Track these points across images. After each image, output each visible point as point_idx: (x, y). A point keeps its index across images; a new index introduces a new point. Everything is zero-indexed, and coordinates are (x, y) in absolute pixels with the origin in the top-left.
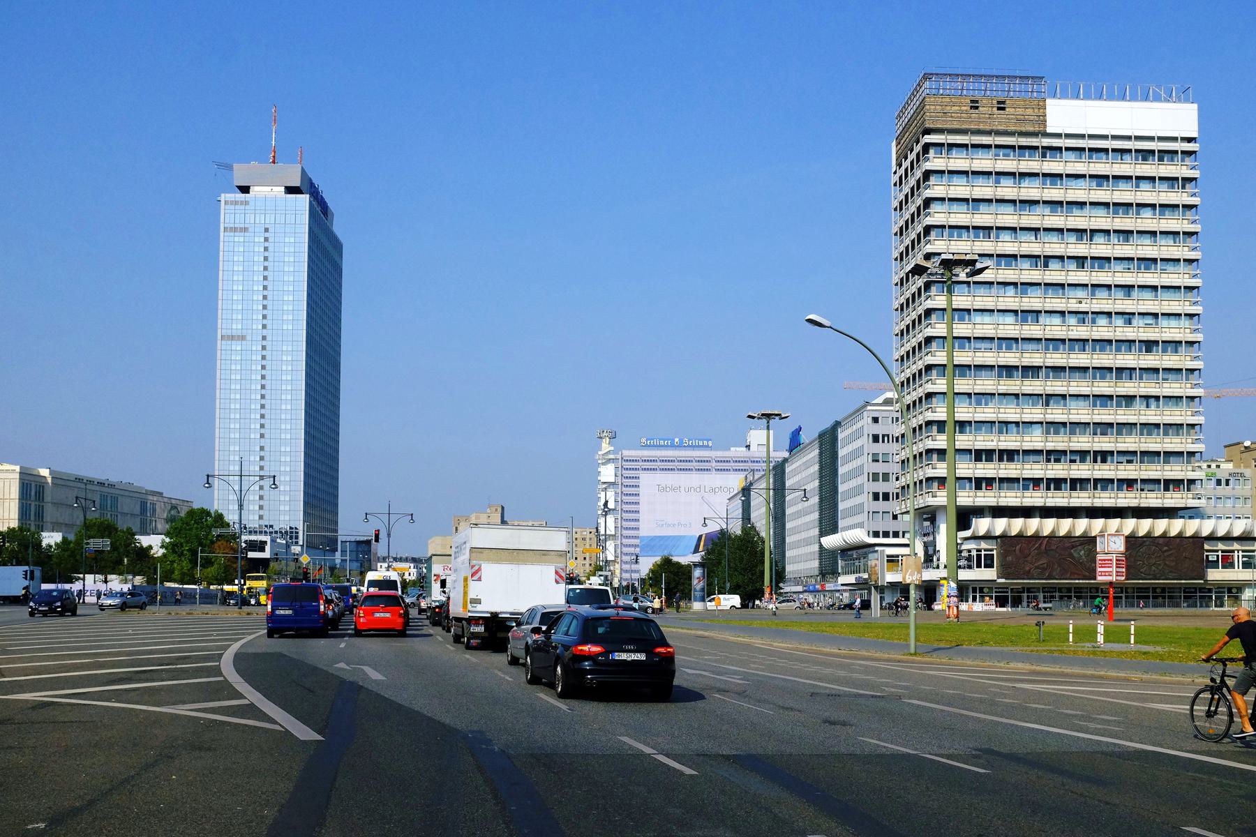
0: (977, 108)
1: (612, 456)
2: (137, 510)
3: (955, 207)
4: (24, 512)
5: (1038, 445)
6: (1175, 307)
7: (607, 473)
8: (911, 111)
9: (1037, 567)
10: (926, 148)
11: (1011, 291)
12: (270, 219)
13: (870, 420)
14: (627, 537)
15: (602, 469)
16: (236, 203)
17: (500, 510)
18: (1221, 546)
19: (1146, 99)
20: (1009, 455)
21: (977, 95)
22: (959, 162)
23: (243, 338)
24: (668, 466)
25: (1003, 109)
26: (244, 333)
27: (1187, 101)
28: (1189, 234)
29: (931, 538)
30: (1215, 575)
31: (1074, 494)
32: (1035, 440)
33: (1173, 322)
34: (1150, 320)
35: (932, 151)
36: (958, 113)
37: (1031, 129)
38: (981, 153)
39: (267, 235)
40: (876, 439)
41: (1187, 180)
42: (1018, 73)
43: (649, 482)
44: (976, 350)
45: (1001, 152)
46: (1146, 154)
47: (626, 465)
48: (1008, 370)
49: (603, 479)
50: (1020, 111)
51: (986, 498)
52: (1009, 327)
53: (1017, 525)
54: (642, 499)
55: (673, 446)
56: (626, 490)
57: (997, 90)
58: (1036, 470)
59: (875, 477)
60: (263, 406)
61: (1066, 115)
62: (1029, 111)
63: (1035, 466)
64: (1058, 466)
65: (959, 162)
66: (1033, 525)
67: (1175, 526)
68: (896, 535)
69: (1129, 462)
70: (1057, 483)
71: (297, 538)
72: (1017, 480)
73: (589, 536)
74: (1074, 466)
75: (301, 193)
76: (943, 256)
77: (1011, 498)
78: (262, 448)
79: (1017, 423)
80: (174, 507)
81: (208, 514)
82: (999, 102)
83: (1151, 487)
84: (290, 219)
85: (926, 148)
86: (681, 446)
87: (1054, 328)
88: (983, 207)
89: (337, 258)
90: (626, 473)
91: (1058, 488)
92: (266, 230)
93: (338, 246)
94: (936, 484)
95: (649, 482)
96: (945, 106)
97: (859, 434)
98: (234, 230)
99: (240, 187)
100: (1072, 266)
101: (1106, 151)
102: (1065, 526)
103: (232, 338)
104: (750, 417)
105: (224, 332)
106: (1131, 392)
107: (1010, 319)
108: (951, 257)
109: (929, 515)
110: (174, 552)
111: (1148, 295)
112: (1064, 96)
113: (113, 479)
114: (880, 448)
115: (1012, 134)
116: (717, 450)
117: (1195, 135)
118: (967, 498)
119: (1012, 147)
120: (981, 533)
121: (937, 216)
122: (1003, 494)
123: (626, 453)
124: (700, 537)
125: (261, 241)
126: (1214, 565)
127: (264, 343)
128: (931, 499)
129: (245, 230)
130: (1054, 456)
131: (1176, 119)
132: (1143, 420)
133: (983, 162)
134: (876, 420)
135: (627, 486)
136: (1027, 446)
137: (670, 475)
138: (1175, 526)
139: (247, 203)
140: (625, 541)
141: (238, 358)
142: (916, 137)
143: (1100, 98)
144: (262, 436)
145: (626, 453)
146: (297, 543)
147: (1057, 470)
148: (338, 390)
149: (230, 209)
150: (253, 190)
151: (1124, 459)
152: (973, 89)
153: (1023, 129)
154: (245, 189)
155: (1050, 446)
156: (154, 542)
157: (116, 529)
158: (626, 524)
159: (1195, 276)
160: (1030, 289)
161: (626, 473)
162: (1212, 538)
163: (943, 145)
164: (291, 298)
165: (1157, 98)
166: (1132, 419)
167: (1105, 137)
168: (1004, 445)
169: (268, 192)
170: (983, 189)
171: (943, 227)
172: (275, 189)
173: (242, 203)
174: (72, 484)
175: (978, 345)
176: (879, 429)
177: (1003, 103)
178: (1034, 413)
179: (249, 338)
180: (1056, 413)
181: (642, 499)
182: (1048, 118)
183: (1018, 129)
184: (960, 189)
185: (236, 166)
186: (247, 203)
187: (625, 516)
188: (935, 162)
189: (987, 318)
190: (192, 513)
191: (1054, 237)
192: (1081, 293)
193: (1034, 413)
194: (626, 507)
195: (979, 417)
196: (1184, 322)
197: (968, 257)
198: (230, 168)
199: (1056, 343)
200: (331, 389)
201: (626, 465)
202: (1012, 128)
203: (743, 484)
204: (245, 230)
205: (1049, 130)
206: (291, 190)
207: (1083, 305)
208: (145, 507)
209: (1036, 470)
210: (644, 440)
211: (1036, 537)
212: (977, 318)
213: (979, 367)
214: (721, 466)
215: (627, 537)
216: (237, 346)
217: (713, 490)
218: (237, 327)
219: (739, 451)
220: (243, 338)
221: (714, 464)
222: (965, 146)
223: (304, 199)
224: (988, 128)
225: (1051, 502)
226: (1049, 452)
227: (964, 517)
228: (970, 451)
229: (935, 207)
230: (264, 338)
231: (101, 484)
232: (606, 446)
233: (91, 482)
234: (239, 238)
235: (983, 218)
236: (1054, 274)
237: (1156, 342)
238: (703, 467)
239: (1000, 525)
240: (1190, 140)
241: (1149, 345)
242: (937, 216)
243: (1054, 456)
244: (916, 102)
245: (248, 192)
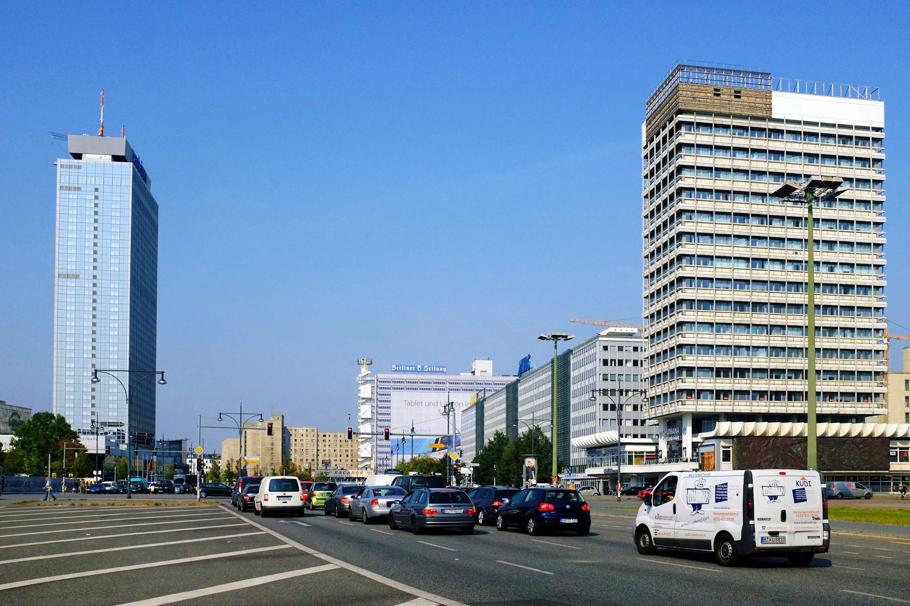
0: (719, 95)
1: (369, 378)
3: (702, 174)
5: (764, 365)
6: (866, 260)
7: (366, 391)
8: (662, 97)
9: (765, 461)
10: (679, 125)
11: (743, 242)
12: (99, 181)
13: (601, 348)
14: (381, 446)
15: (361, 388)
16: (70, 167)
17: (281, 418)
18: (899, 445)
19: (845, 95)
20: (741, 372)
21: (719, 85)
22: (704, 138)
23: (77, 277)
24: (412, 386)
25: (739, 97)
26: (78, 272)
27: (875, 98)
28: (876, 203)
29: (677, 438)
30: (896, 466)
31: (791, 403)
32: (761, 361)
33: (865, 271)
34: (847, 269)
35: (683, 128)
36: (705, 99)
37: (760, 114)
38: (721, 132)
40: (605, 363)
41: (876, 161)
42: (750, 69)
43: (397, 398)
44: (718, 288)
45: (737, 132)
46: (846, 139)
48: (741, 305)
50: (752, 100)
51: (724, 406)
52: (742, 271)
53: (749, 428)
54: (392, 411)
55: (416, 371)
56: (380, 404)
57: (728, 84)
58: (762, 384)
59: (605, 392)
60: (94, 332)
61: (787, 105)
62: (759, 100)
63: (760, 382)
64: (778, 382)
65: (704, 138)
66: (762, 428)
67: (855, 429)
68: (643, 436)
69: (831, 379)
70: (777, 395)
71: (123, 438)
72: (748, 392)
74: (790, 382)
75: (126, 161)
76: (814, 178)
77: (743, 406)
79: (748, 348)
80: (15, 413)
81: (52, 417)
82: (736, 92)
83: (847, 398)
84: (117, 182)
85: (679, 125)
86: (422, 371)
87: (774, 273)
88: (723, 175)
89: (153, 216)
91: (778, 399)
92: (96, 190)
93: (155, 207)
94: (685, 395)
95: (397, 398)
96: (694, 92)
97: (592, 358)
98: (69, 188)
100: (790, 224)
101: (816, 135)
102: (785, 428)
104: (542, 338)
105: (61, 272)
106: (834, 325)
107: (742, 264)
108: (819, 178)
109: (673, 422)
110: (23, 448)
111: (846, 249)
112: (785, 90)
114: (609, 370)
115: (745, 117)
116: (450, 374)
117: (882, 125)
118: (706, 406)
119: (745, 128)
120: (722, 434)
121: (688, 180)
122: (736, 403)
123: (380, 376)
125: (91, 200)
126: (894, 459)
127: (95, 281)
128: (680, 406)
129: (79, 189)
130: (777, 373)
131: (868, 113)
132: (843, 346)
133: (723, 139)
134: (605, 348)
135: (381, 402)
136: (756, 366)
137: (414, 393)
138: (855, 429)
139: (79, 167)
142: (668, 119)
143: (811, 92)
144: (94, 356)
145: (380, 376)
146: (123, 442)
147: (777, 385)
149: (65, 172)
151: (828, 376)
152: (716, 80)
153: (754, 114)
154: (78, 156)
155: (773, 366)
159: (880, 235)
160: (758, 242)
162: (894, 438)
163: (692, 123)
165: (854, 96)
166: (834, 346)
167: (816, 124)
168: (738, 365)
169: (97, 159)
170: (723, 161)
171: (693, 189)
172: (104, 157)
173: (75, 167)
175: (718, 285)
176: (608, 355)
177: (739, 92)
178: (761, 340)
179: (82, 276)
180: (777, 340)
181: (392, 411)
182: (773, 106)
183: (750, 113)
184: (705, 159)
185: (69, 136)
186: (79, 167)
188: (686, 137)
189: (725, 264)
190: (38, 416)
191: (706, 219)
192: (796, 246)
193: (761, 340)
194: (380, 417)
195: (719, 342)
196: (873, 271)
197: (834, 180)
198: (66, 139)
199: (778, 284)
200: (150, 321)
202: (746, 113)
203: (475, 400)
204: (79, 189)
205: (774, 116)
206: (116, 158)
207: (798, 255)
209: (762, 384)
210: (394, 366)
211: (764, 437)
212: (718, 264)
213: (719, 302)
215: (381, 446)
216: (72, 283)
218: (72, 268)
219: (467, 376)
220: (77, 277)
221: (448, 385)
222: (709, 125)
223: (129, 166)
224: (727, 111)
225: (773, 410)
226: (772, 370)
227: (702, 422)
228: (711, 369)
229: (685, 173)
230: (95, 277)
232: (364, 370)
234: (73, 195)
235: (723, 184)
236: (776, 230)
237: (852, 286)
239: (737, 428)
240: (877, 129)
241: (847, 288)
242: (688, 180)
243: (777, 373)
244: (668, 89)
245: (80, 158)
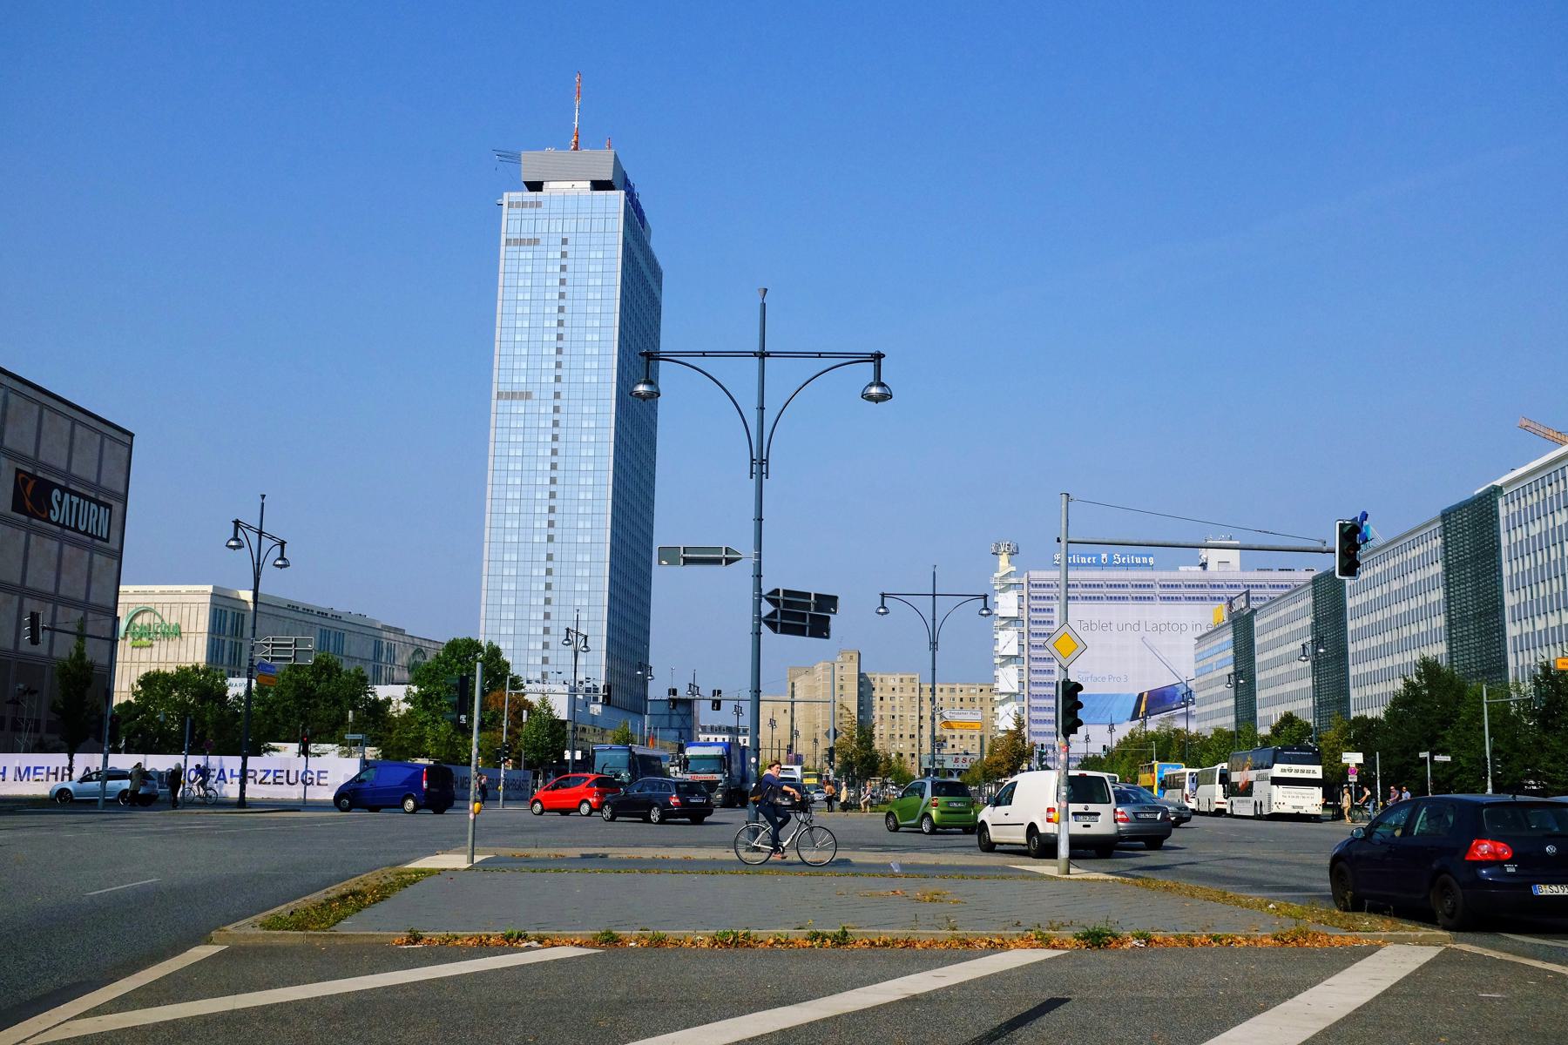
1: (1013, 580)
2: (369, 654)
4: (214, 650)
12: (570, 226)
14: (1036, 696)
16: (524, 205)
17: (856, 657)
23: (527, 396)
24: (1116, 594)
39: (565, 248)
47: (1036, 592)
49: (1001, 612)
73: (979, 695)
75: (613, 188)
78: (550, 557)
84: (598, 225)
89: (654, 286)
90: (1035, 604)
92: (565, 242)
93: (657, 273)
98: (520, 242)
99: (527, 184)
103: (512, 396)
113: (340, 608)
123: (1034, 574)
124: (1141, 696)
125: (556, 259)
129: (536, 242)
139: (538, 204)
140: (1034, 702)
141: (521, 424)
144: (550, 539)
145: (1034, 574)
146: (596, 699)
148: (653, 477)
149: (516, 214)
150: (549, 186)
154: (535, 186)
156: (395, 694)
157: (339, 671)
158: (1035, 677)
161: (1035, 604)
164: (596, 338)
172: (578, 184)
174: (281, 612)
179: (535, 395)
185: (525, 155)
186: (538, 204)
187: (1035, 665)
201: (1036, 592)
204: (536, 242)
206: (598, 185)
208: (379, 644)
214: (1146, 592)
215: (1036, 696)
216: (519, 407)
217: (1157, 628)
220: (527, 396)
221: (1158, 590)
223: (618, 196)
230: (557, 395)
231: (323, 614)
233: (308, 611)
238: (1173, 593)
245: (540, 189)
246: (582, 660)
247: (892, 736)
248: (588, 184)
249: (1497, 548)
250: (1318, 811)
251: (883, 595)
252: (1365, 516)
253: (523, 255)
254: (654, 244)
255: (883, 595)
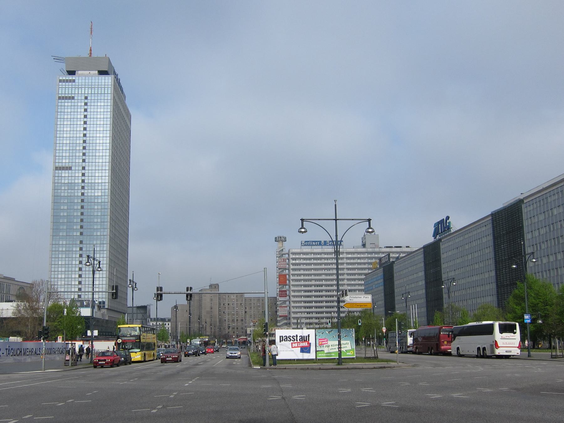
23: (70, 168)
92: (86, 98)
186: (74, 81)
220: (70, 168)
230: (84, 168)
246: (97, 276)
247: (233, 321)
248: (97, 72)
249: (522, 227)
250: (516, 352)
251: (302, 220)
252: (448, 218)
253: (66, 104)
254: (127, 102)
255: (302, 220)
